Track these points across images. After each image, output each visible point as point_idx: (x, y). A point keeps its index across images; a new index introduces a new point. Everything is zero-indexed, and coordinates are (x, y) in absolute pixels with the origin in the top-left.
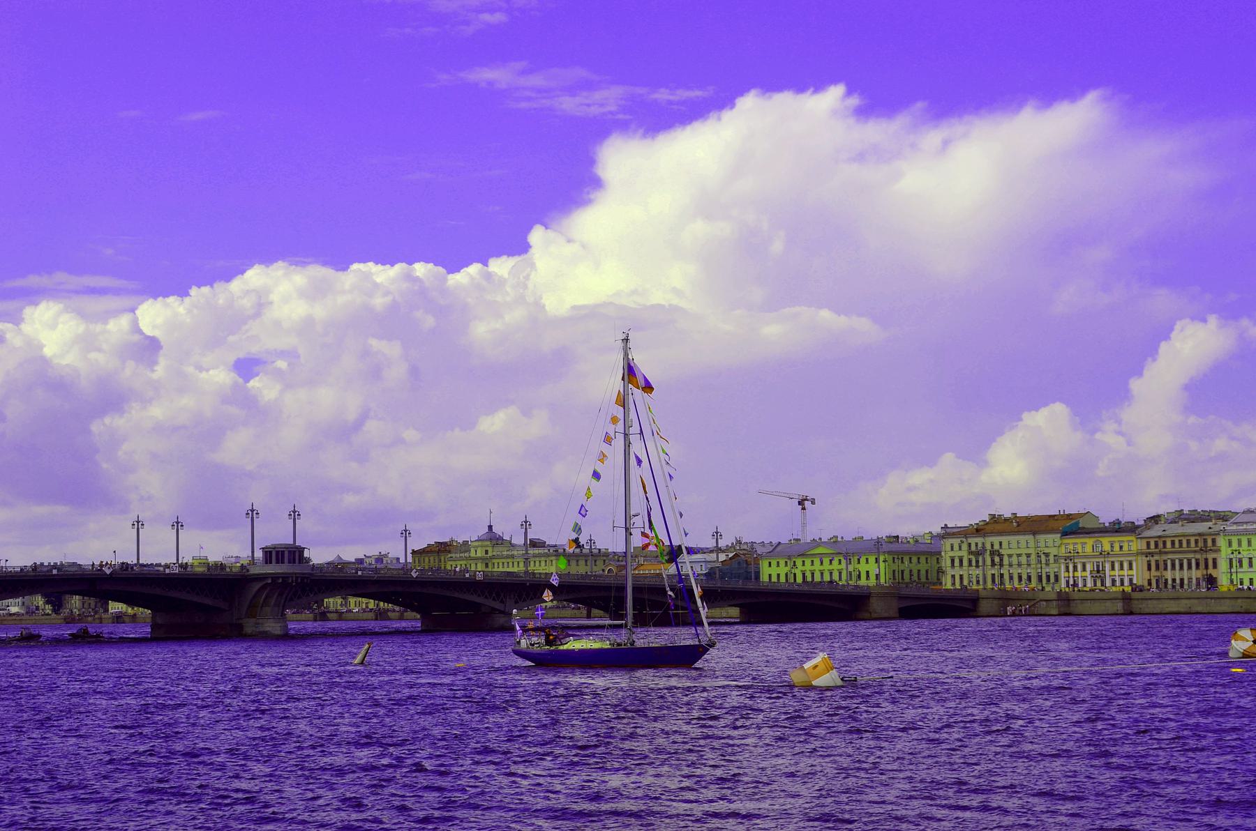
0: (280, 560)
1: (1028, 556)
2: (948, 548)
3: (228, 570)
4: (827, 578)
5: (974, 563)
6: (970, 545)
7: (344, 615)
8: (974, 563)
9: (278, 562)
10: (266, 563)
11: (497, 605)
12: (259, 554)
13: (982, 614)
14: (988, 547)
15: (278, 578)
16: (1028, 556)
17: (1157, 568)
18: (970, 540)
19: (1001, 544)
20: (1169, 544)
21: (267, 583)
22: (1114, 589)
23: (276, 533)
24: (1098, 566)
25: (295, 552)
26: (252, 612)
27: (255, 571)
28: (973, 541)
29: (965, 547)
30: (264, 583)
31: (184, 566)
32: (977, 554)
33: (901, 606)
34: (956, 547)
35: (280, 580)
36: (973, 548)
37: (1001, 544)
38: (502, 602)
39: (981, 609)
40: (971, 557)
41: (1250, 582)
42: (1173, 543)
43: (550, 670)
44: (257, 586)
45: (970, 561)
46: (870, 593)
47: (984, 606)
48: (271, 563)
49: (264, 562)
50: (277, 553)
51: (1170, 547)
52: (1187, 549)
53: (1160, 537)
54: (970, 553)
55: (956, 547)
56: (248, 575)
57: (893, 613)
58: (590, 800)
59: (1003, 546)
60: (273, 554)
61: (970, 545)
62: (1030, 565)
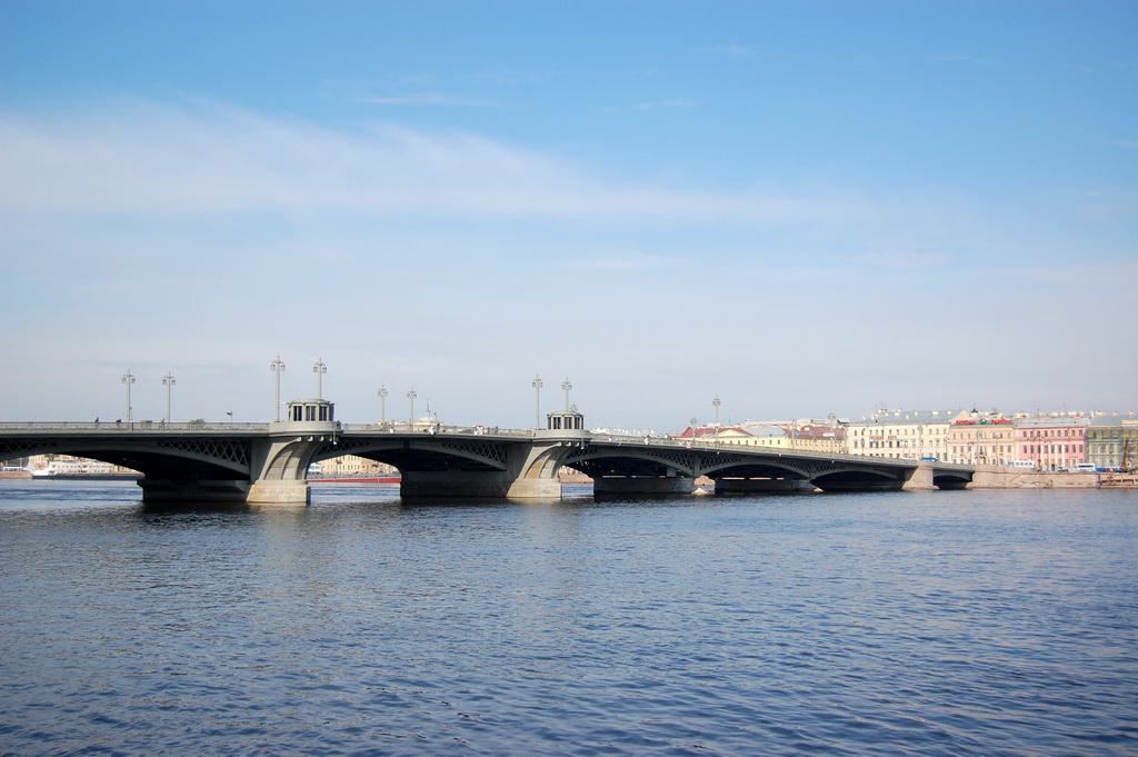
11: (687, 470)
14: (887, 433)
16: (914, 441)
18: (1054, 443)
28: (874, 428)
48: (300, 419)
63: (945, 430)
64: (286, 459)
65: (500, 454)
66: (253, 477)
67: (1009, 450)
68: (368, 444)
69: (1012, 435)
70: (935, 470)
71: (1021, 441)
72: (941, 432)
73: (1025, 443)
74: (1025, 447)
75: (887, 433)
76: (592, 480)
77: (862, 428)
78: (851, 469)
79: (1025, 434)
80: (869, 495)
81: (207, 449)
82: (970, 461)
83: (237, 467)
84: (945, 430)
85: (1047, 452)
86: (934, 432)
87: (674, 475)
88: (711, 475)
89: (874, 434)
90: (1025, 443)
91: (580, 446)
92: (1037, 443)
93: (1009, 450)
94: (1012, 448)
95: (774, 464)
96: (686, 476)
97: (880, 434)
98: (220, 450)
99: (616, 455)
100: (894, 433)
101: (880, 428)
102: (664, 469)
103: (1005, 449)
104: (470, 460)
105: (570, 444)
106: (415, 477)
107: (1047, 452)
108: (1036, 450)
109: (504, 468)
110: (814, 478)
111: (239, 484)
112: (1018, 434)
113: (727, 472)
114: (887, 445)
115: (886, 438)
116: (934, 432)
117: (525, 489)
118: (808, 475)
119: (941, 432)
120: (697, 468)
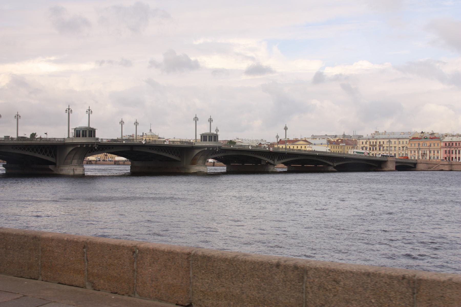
0: (84, 135)
1: (395, 147)
2: (361, 143)
3: (100, 141)
4: (401, 155)
5: (372, 149)
6: (370, 142)
7: (98, 162)
8: (372, 149)
9: (209, 141)
10: (77, 136)
11: (272, 162)
12: (199, 137)
13: (419, 170)
14: (378, 143)
15: (84, 145)
16: (395, 147)
17: (449, 153)
18: (370, 141)
19: (383, 142)
20: (454, 144)
21: (205, 150)
22: (434, 160)
23: (204, 129)
24: (424, 152)
25: (216, 136)
26: (194, 162)
27: (197, 144)
28: (371, 141)
29: (368, 143)
30: (76, 147)
31: (23, 138)
32: (373, 146)
33: (397, 165)
34: (364, 143)
35: (85, 146)
36: (372, 143)
37: (383, 142)
38: (273, 160)
39: (418, 167)
40: (370, 147)
41: (460, 159)
42: (456, 144)
43: (115, 182)
44: (71, 149)
45: (370, 148)
46: (388, 160)
47: (420, 166)
48: (206, 141)
49: (76, 136)
50: (204, 136)
51: (414, 146)
52: (433, 147)
53: (451, 142)
54: (370, 145)
55: (364, 143)
56: (195, 146)
57: (394, 169)
58: (3, 228)
59: (385, 143)
60: (79, 133)
61: (370, 142)
62: (395, 151)
63: (406, 142)
64: (73, 155)
65: (272, 158)
66: (58, 164)
67: (438, 152)
68: (113, 148)
69: (439, 145)
70: (396, 162)
71: (443, 148)
72: (405, 143)
73: (446, 149)
74: (446, 151)
75: (378, 143)
76: (4, 168)
77: (366, 141)
78: (240, 154)
79: (446, 144)
80: (375, 172)
81: (39, 151)
82: (415, 157)
83: (50, 159)
84: (395, 142)
85: (456, 153)
86: (401, 143)
87: (265, 164)
88: (285, 164)
89: (372, 143)
90: (446, 149)
91: (216, 149)
92: (449, 149)
93: (438, 152)
94: (439, 152)
95: (315, 159)
96: (271, 164)
97: (375, 143)
98: (41, 151)
99: (303, 158)
100: (382, 143)
101: (375, 141)
102: (260, 161)
103: (436, 152)
104: (170, 158)
105: (211, 149)
106: (136, 164)
107: (456, 153)
108: (451, 152)
109: (180, 160)
110: (335, 166)
111: (51, 167)
112: (443, 144)
113: (293, 162)
114: (378, 149)
115: (378, 145)
116: (401, 143)
117: (62, 170)
118: (332, 164)
119: (405, 143)
120: (276, 160)
